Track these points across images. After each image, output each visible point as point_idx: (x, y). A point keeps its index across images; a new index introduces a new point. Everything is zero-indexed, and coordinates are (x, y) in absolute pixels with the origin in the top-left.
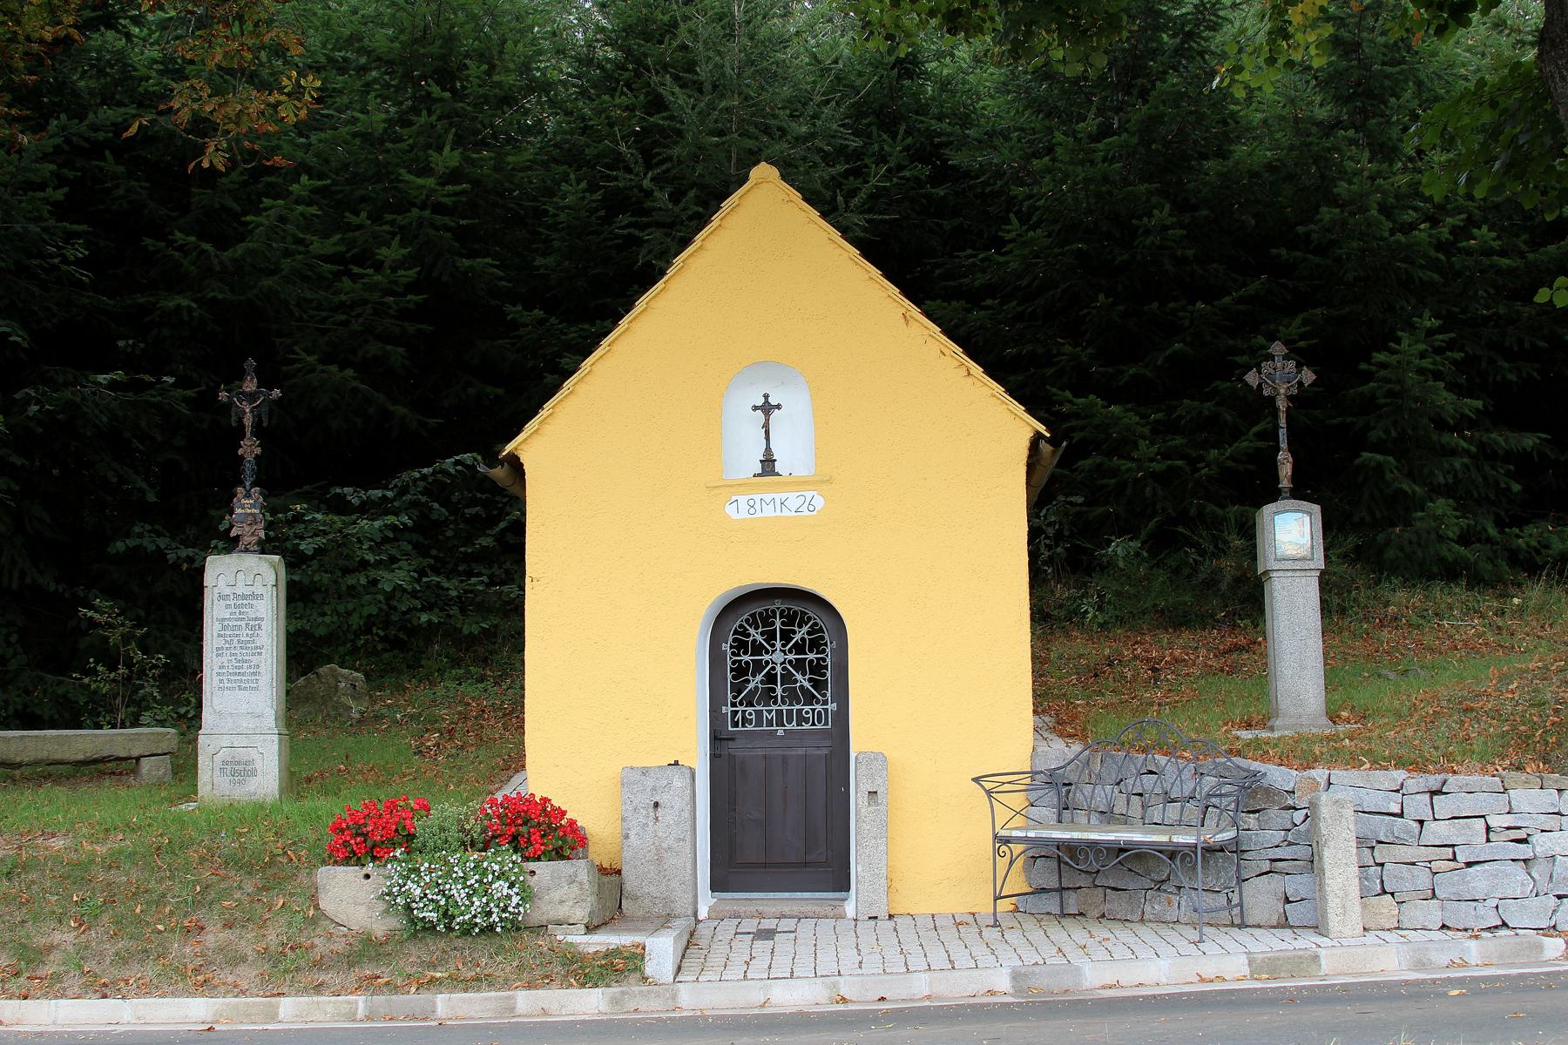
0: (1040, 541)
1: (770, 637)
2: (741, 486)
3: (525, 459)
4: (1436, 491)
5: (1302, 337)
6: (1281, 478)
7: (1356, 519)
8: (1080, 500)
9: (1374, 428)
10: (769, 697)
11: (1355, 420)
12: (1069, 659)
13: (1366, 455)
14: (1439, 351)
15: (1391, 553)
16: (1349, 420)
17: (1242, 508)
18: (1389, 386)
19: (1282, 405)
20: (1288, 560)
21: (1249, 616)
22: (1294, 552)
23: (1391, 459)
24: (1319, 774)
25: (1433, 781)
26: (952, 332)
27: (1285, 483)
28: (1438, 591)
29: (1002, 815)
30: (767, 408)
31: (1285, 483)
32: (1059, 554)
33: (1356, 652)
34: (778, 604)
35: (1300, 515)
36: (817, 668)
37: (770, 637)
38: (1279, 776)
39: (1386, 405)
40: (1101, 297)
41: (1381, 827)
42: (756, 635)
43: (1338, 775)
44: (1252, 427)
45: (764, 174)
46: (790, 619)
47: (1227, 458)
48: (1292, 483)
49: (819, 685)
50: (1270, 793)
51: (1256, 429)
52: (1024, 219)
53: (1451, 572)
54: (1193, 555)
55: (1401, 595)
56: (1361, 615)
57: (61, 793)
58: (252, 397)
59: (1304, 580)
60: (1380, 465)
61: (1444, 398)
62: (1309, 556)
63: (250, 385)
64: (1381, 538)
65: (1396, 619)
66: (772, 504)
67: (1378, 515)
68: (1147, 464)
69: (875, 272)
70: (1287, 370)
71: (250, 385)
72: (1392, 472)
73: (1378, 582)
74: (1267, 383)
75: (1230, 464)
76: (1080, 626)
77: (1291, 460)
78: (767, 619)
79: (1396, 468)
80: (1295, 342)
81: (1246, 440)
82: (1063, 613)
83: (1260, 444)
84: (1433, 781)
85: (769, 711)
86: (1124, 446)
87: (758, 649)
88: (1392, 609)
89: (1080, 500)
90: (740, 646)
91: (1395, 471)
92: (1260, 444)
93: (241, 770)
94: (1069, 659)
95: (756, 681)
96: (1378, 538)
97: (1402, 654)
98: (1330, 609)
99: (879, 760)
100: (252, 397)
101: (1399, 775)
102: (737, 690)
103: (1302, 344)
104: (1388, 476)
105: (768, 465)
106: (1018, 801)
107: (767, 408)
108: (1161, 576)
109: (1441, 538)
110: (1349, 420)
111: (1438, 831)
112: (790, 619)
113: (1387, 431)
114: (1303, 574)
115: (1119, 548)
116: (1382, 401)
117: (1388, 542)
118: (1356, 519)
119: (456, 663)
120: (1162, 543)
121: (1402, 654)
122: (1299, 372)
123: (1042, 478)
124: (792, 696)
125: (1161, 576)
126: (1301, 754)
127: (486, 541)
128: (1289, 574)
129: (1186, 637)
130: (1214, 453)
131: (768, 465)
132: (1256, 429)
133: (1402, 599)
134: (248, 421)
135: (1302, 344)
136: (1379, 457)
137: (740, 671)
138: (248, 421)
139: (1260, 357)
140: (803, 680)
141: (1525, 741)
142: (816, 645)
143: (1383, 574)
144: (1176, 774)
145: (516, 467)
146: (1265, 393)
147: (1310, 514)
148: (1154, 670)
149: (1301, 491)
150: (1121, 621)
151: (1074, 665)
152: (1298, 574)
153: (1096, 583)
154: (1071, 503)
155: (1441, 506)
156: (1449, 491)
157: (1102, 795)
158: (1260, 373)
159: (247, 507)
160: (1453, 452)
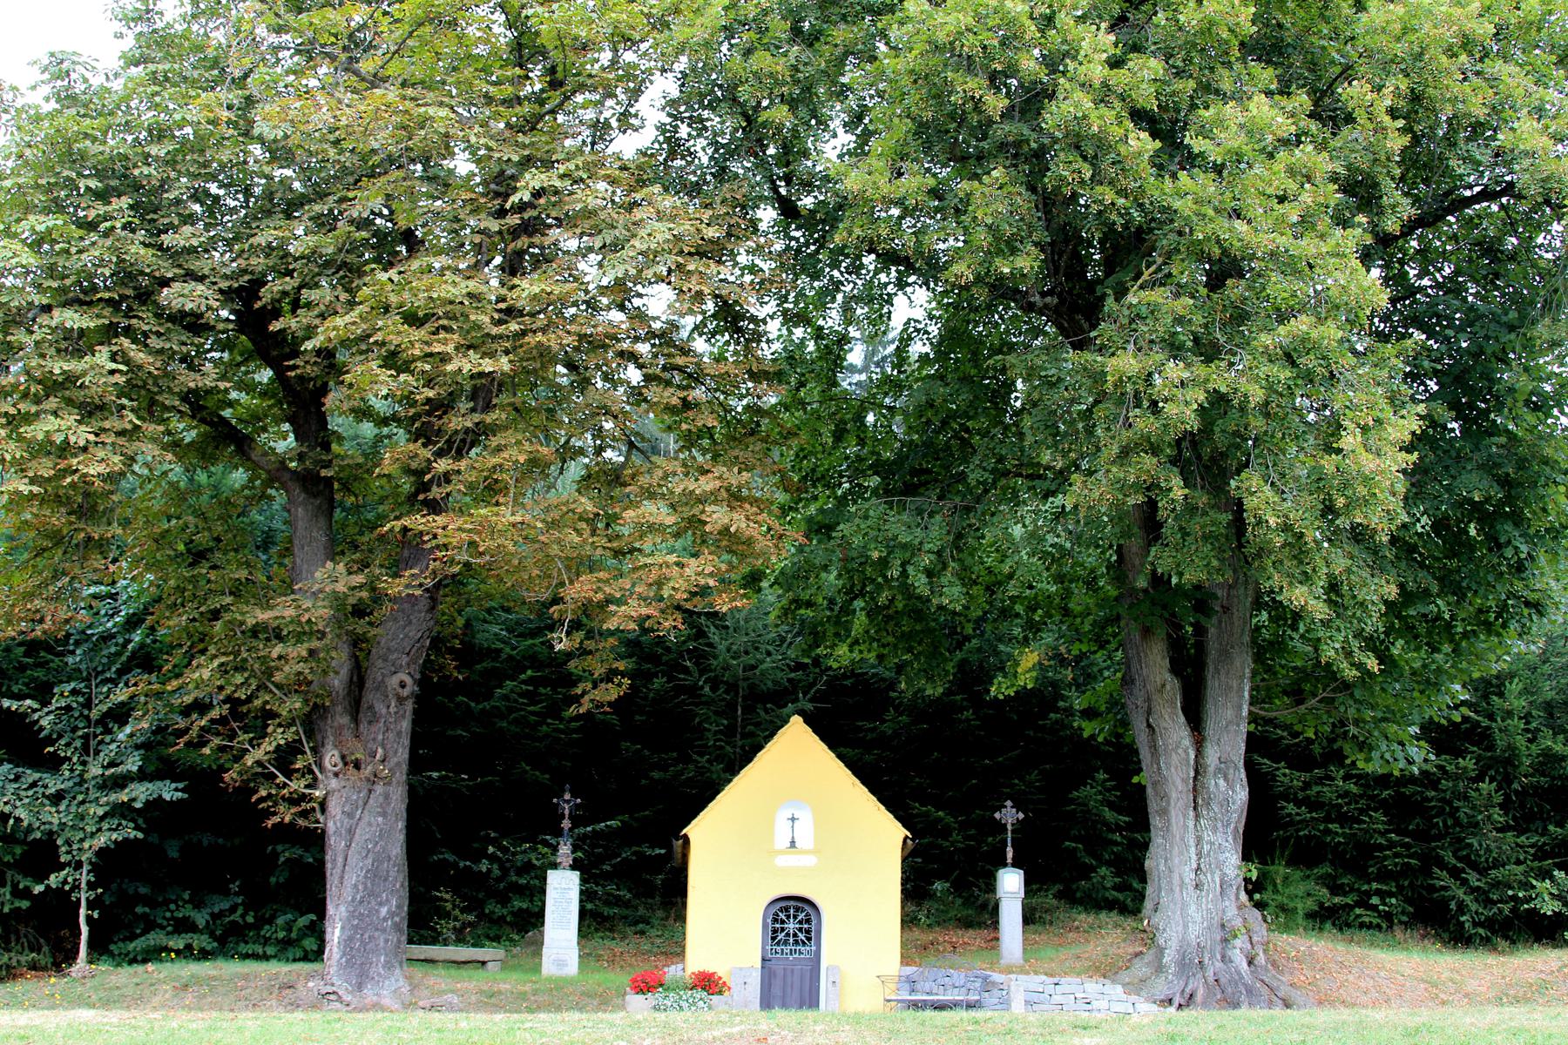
1: (788, 917)
2: (781, 852)
3: (691, 836)
4: (1102, 862)
10: (786, 943)
14: (1108, 790)
15: (1078, 895)
19: (1009, 827)
24: (1013, 976)
25: (1056, 980)
26: (840, 757)
27: (1009, 861)
28: (1103, 915)
29: (887, 991)
30: (793, 819)
31: (1009, 861)
34: (792, 903)
36: (808, 931)
37: (788, 917)
38: (997, 977)
41: (1035, 997)
42: (782, 916)
43: (1021, 977)
45: (797, 720)
46: (797, 909)
49: (809, 939)
50: (994, 983)
52: (896, 708)
53: (1110, 905)
54: (977, 892)
55: (1083, 916)
57: (453, 972)
58: (568, 802)
61: (1109, 814)
63: (567, 796)
66: (791, 860)
69: (842, 764)
71: (567, 796)
76: (917, 925)
78: (787, 909)
84: (1056, 980)
85: (787, 949)
86: (946, 833)
87: (783, 922)
90: (775, 920)
93: (561, 963)
95: (781, 936)
98: (1029, 918)
99: (832, 969)
100: (568, 802)
101: (1044, 977)
102: (773, 939)
105: (793, 844)
106: (893, 986)
107: (793, 819)
108: (959, 901)
109: (1105, 888)
111: (1057, 999)
112: (797, 909)
115: (938, 886)
119: (597, 930)
120: (959, 887)
123: (907, 851)
124: (796, 942)
125: (959, 901)
126: (1009, 970)
127: (607, 867)
129: (971, 932)
131: (793, 844)
133: (1083, 919)
134: (567, 812)
137: (775, 931)
138: (567, 812)
139: (1000, 808)
140: (801, 936)
141: (1097, 969)
142: (808, 921)
144: (958, 977)
145: (686, 840)
149: (1016, 864)
150: (939, 924)
153: (927, 904)
155: (1103, 871)
156: (1108, 864)
157: (927, 987)
159: (565, 850)
160: (1116, 843)
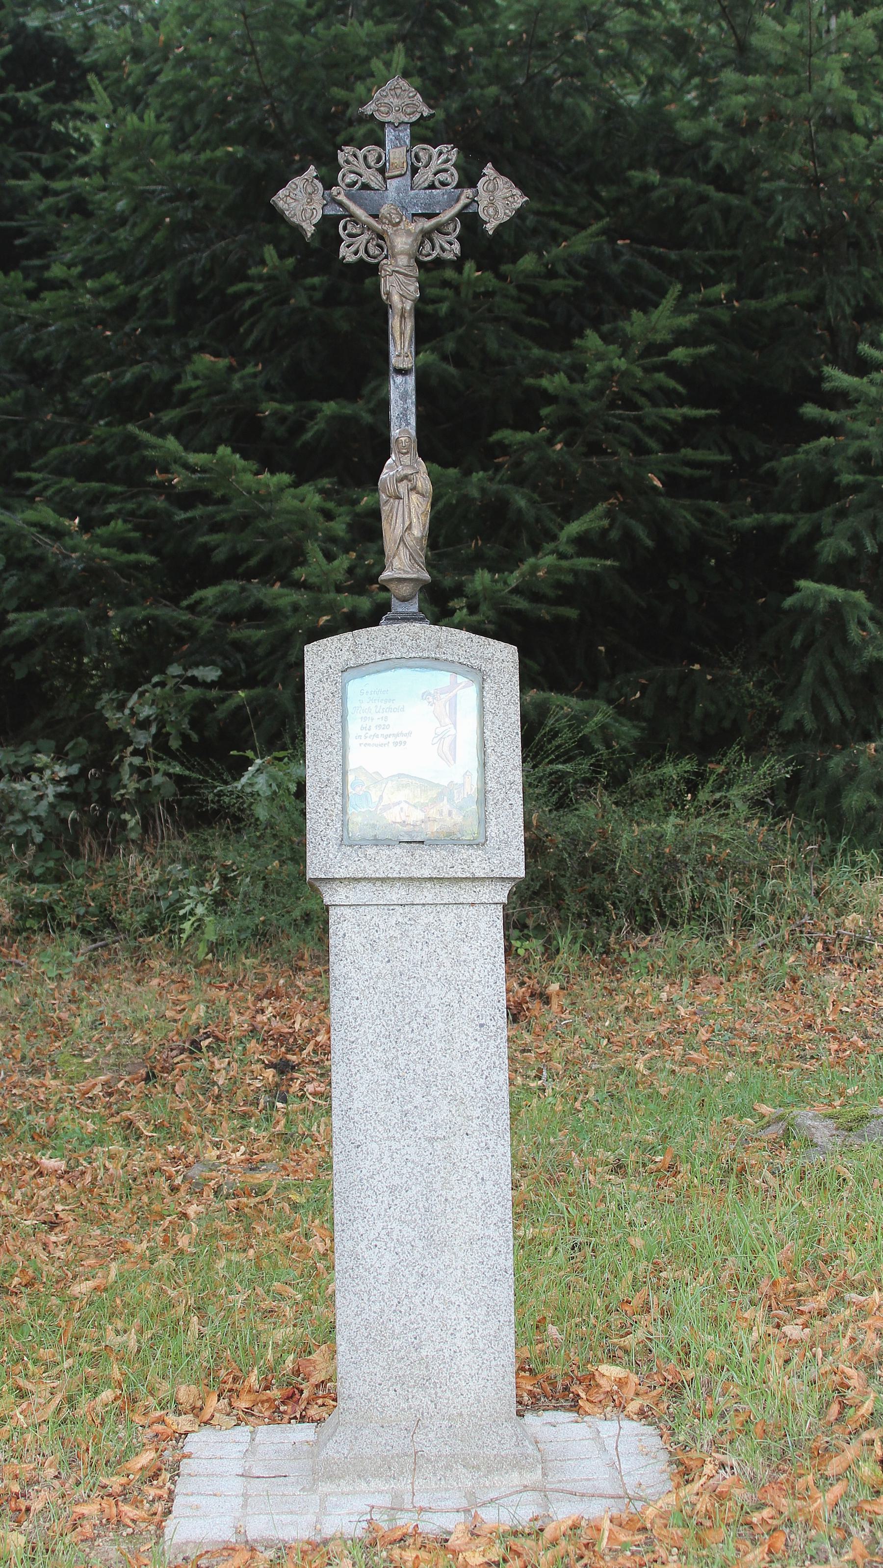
0: (122, 759)
5: (681, 338)
6: (389, 544)
7: (787, 725)
8: (211, 674)
9: (830, 535)
11: (789, 518)
12: (111, 1031)
13: (807, 585)
16: (777, 518)
17: (543, 695)
18: (858, 443)
20: (388, 843)
21: (540, 930)
22: (416, 816)
23: (859, 595)
32: (158, 788)
33: (761, 1030)
35: (442, 678)
39: (856, 488)
40: (270, 252)
44: (568, 520)
47: (516, 591)
48: (430, 565)
51: (574, 528)
56: (785, 932)
59: (448, 918)
60: (835, 606)
62: (471, 830)
64: (836, 764)
65: (860, 943)
67: (834, 715)
68: (332, 595)
70: (425, 176)
72: (862, 625)
73: (828, 860)
74: (356, 221)
75: (521, 604)
77: (424, 482)
79: (872, 618)
80: (664, 348)
81: (552, 552)
82: (140, 917)
83: (583, 563)
88: (852, 920)
89: (211, 674)
91: (870, 624)
92: (583, 563)
94: (111, 1031)
96: (832, 764)
97: (866, 1036)
103: (679, 353)
104: (855, 633)
110: (777, 518)
113: (855, 539)
114: (446, 894)
116: (846, 478)
117: (852, 774)
118: (787, 725)
121: (866, 1036)
122: (469, 179)
128: (396, 894)
130: (482, 579)
132: (574, 528)
135: (679, 353)
136: (835, 592)
143: (839, 840)
146: (347, 254)
147: (480, 676)
148: (284, 1068)
151: (116, 1046)
152: (428, 894)
154: (193, 681)
158: (329, 183)
